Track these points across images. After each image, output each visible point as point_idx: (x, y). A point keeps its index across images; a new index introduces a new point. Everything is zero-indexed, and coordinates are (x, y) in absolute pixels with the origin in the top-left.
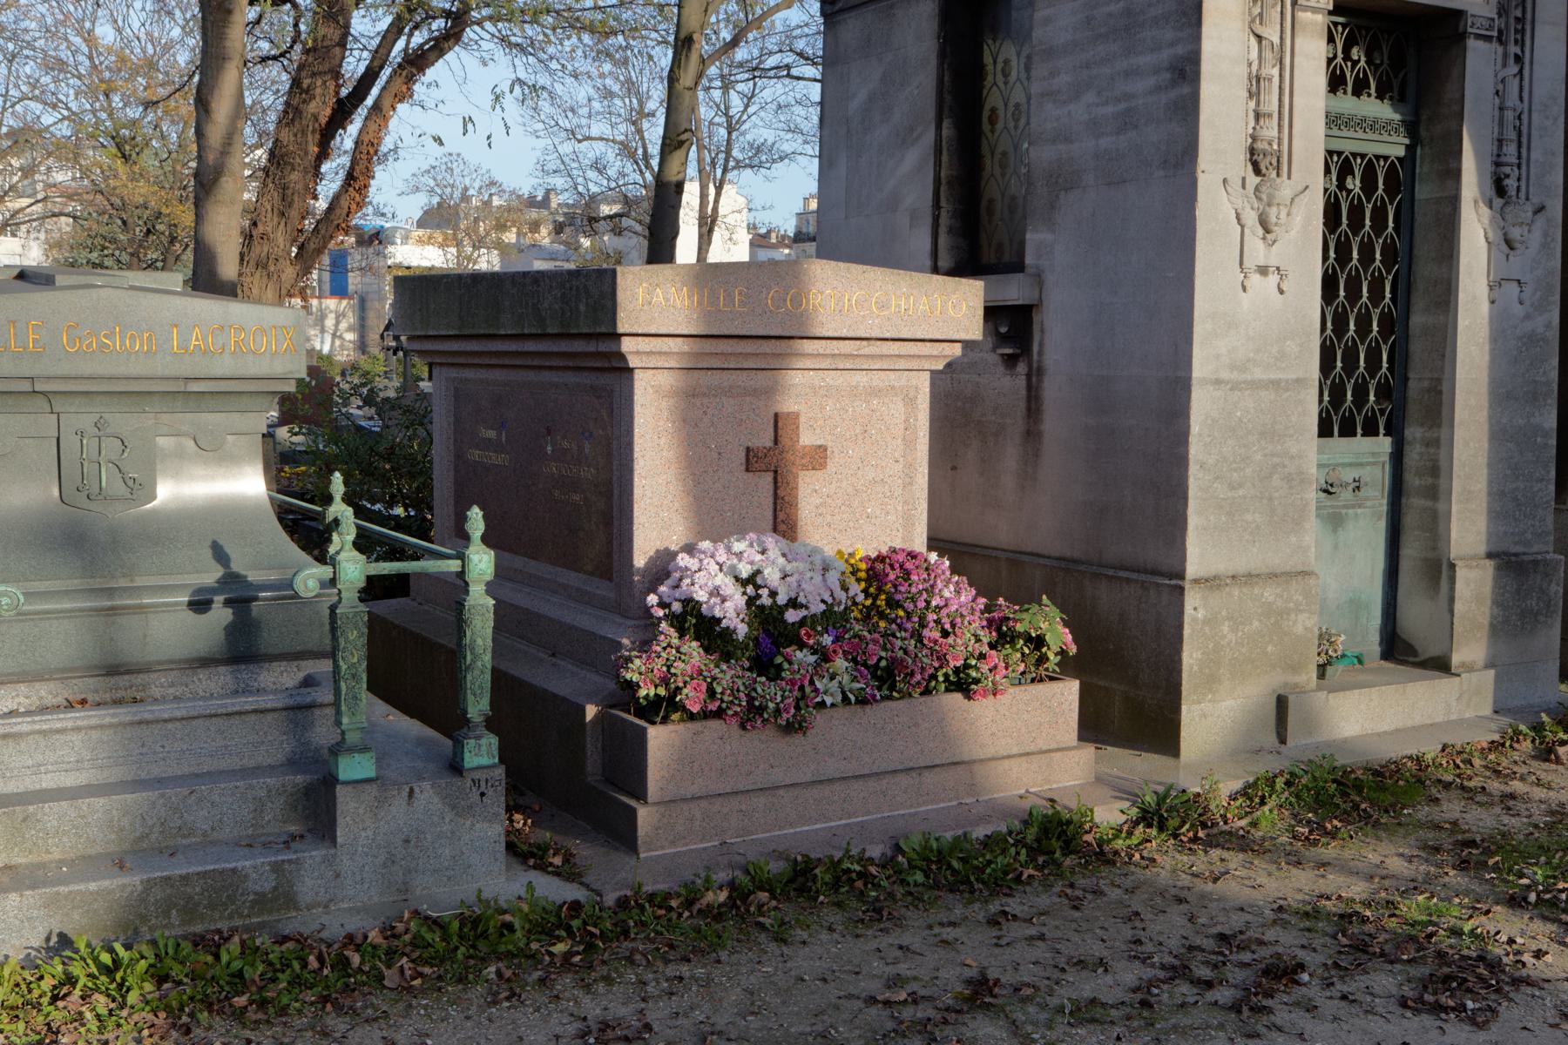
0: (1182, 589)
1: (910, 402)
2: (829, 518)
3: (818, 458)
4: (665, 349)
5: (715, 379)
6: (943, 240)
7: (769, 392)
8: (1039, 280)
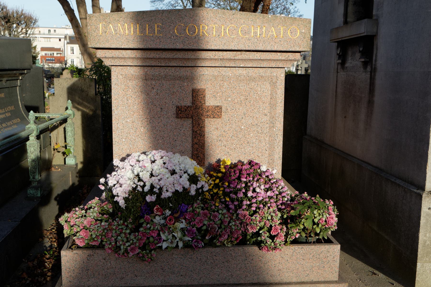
0: (421, 197)
1: (273, 84)
2: (225, 143)
3: (217, 112)
4: (121, 56)
5: (157, 71)
6: (351, 8)
7: (191, 79)
8: (377, 22)
